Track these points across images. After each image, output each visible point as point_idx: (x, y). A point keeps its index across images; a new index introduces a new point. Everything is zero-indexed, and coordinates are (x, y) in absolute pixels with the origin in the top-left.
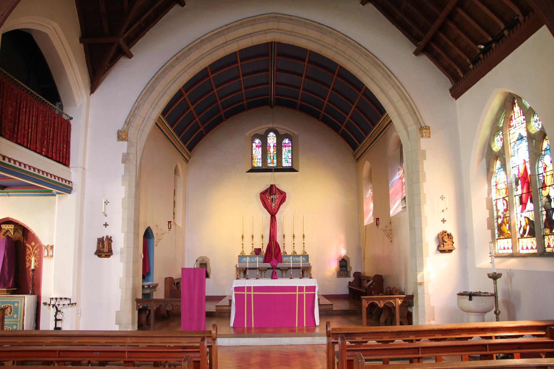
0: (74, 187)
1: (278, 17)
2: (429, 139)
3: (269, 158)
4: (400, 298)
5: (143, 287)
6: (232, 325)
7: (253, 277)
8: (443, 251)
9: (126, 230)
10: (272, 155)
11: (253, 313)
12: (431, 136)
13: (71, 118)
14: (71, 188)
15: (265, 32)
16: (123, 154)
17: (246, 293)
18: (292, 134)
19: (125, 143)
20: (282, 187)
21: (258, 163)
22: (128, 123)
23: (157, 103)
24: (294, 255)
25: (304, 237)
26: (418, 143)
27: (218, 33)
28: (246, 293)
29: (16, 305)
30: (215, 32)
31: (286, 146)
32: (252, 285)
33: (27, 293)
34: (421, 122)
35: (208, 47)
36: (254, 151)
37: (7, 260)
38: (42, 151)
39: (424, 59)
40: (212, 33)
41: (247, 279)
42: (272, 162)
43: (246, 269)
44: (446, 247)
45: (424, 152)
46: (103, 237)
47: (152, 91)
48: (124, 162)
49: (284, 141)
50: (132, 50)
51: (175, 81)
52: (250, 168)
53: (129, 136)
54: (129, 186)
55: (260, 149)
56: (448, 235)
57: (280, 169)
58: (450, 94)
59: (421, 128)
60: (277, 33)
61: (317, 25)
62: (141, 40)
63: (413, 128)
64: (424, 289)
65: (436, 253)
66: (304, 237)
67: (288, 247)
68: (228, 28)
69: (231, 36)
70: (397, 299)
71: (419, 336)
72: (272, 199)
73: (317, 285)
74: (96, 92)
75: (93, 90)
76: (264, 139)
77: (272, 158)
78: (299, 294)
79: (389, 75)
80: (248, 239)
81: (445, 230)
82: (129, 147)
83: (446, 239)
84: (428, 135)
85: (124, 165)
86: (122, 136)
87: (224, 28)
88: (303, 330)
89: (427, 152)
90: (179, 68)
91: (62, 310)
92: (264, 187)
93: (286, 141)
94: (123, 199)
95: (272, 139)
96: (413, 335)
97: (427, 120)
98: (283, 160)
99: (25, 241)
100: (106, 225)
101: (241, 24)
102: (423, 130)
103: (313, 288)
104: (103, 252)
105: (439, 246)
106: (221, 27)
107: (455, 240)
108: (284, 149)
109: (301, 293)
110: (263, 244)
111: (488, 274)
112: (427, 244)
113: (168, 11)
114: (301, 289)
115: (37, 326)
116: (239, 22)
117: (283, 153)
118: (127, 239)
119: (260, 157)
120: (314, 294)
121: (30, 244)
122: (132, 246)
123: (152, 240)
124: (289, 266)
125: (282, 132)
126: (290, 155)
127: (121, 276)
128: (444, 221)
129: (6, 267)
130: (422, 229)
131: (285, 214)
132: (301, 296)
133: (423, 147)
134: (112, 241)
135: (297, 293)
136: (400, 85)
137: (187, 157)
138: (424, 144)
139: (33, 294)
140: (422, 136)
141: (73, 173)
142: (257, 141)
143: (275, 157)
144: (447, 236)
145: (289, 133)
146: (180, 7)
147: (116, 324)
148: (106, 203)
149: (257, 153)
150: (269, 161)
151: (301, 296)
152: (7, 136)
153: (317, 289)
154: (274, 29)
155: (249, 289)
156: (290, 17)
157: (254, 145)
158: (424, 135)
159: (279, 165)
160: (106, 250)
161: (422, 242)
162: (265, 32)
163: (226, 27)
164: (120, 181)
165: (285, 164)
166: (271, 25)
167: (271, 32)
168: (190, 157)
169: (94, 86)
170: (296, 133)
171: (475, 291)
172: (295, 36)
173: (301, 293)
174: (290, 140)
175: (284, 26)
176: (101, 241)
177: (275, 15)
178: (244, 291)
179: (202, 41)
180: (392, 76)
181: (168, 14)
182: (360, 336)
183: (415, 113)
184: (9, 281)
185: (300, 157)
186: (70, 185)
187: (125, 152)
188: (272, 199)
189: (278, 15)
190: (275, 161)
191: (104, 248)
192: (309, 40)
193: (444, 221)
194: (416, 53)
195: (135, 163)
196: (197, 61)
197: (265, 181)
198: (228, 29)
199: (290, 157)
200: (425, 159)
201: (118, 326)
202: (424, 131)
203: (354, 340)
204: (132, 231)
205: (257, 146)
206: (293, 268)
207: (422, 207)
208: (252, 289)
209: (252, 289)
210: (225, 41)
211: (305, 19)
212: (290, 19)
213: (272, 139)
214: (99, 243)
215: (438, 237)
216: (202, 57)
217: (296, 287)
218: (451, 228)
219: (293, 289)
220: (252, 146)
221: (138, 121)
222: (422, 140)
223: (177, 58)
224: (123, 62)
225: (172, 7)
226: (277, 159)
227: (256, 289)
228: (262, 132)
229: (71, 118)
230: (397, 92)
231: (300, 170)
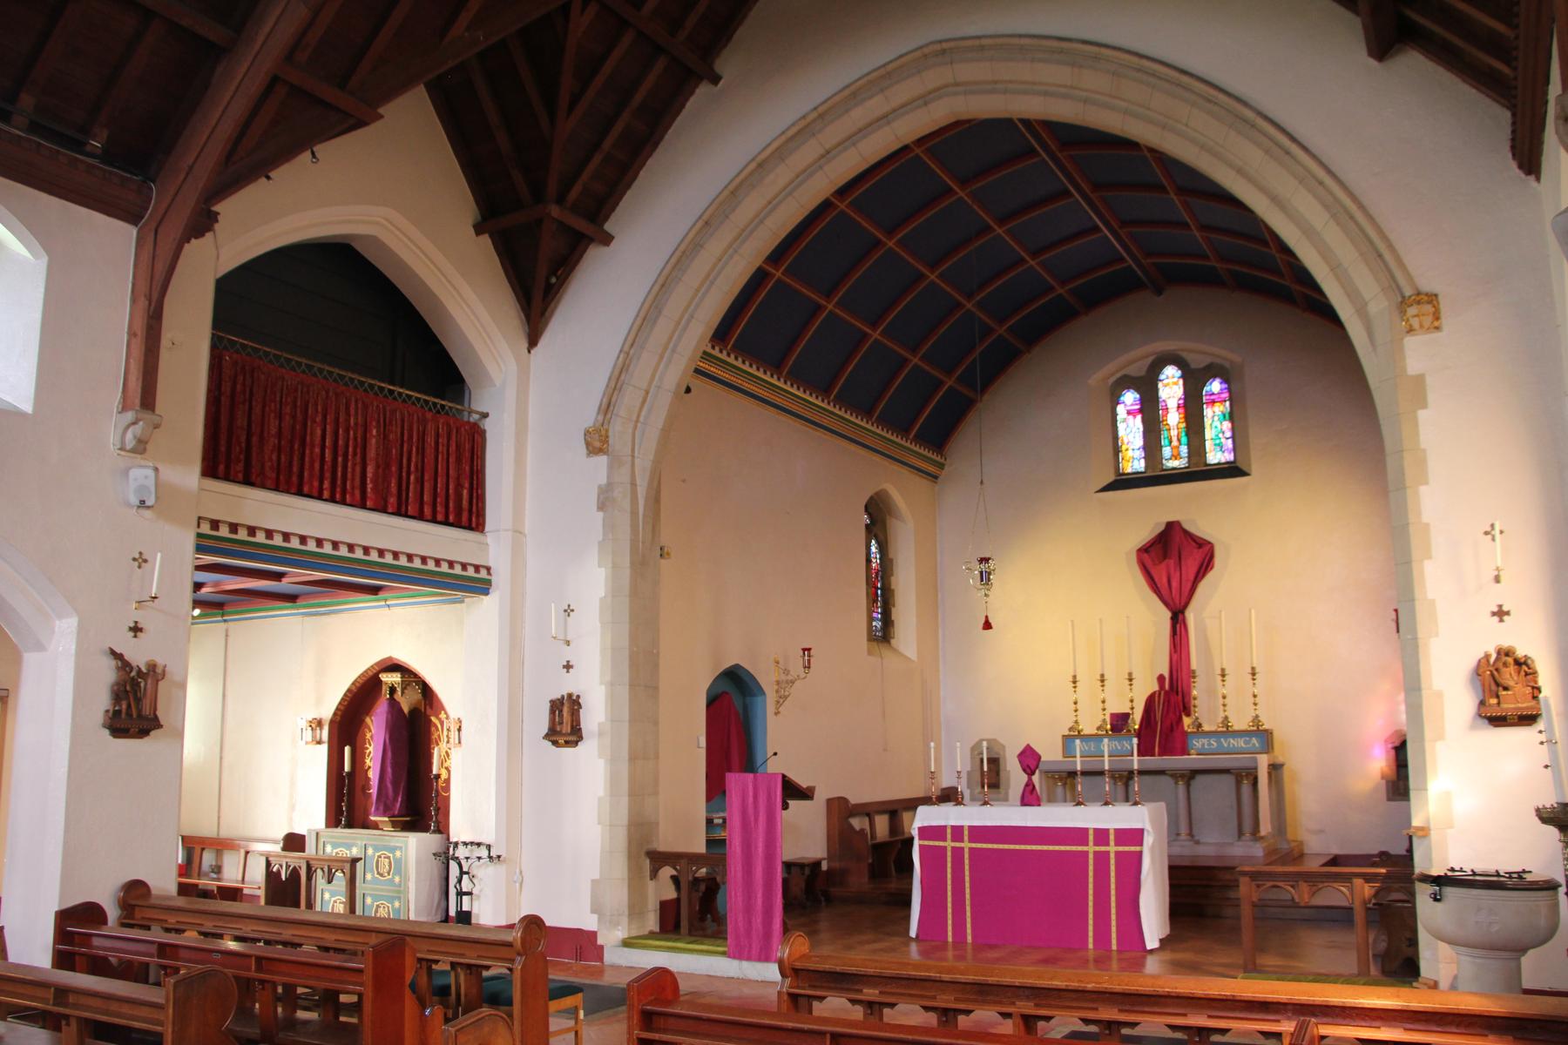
0: (494, 579)
1: (945, 52)
2: (1436, 335)
3: (1164, 442)
4: (1368, 878)
5: (709, 822)
6: (913, 934)
7: (1094, 800)
8: (1498, 721)
9: (608, 678)
10: (1174, 433)
11: (968, 902)
12: (1445, 321)
13: (485, 415)
14: (489, 582)
15: (925, 99)
16: (600, 487)
17: (949, 844)
18: (1227, 365)
19: (602, 460)
20: (1201, 526)
21: (1134, 461)
22: (607, 408)
23: (676, 346)
24: (1227, 731)
25: (1223, 675)
26: (1397, 354)
27: (799, 132)
28: (1091, 849)
29: (398, 854)
30: (790, 133)
31: (1213, 402)
32: (966, 823)
33: (425, 829)
34: (1402, 282)
35: (780, 176)
36: (1121, 427)
37: (389, 754)
38: (386, 502)
39: (1412, 64)
40: (784, 138)
41: (1079, 804)
42: (1174, 457)
43: (1131, 772)
44: (1509, 706)
45: (1420, 380)
46: (1487, 656)
47: (657, 317)
48: (601, 507)
49: (1206, 389)
50: (608, 227)
51: (712, 283)
52: (1111, 478)
53: (611, 441)
54: (615, 566)
55: (1139, 417)
56: (1518, 663)
57: (1199, 472)
58: (1514, 165)
59: (1403, 304)
60: (956, 94)
61: (1055, 44)
62: (629, 193)
63: (1379, 305)
64: (1429, 848)
65: (1473, 727)
66: (1223, 675)
67: (1221, 703)
68: (823, 115)
69: (833, 133)
70: (1358, 882)
71: (1049, 1006)
72: (1174, 563)
73: (1148, 826)
74: (544, 341)
75: (533, 342)
76: (1148, 390)
77: (1175, 443)
78: (1095, 853)
79: (1283, 140)
80: (1087, 681)
81: (1506, 643)
82: (611, 467)
83: (1509, 675)
84: (1427, 320)
85: (601, 514)
86: (597, 442)
87: (809, 119)
88: (1109, 958)
89: (1429, 380)
90: (714, 247)
91: (474, 871)
92: (1145, 532)
93: (1215, 386)
94: (601, 599)
95: (1171, 386)
96: (1028, 998)
97: (1426, 272)
98: (1208, 444)
99: (429, 711)
100: (568, 667)
101: (853, 95)
102: (1419, 306)
103: (1135, 836)
104: (560, 733)
105: (1482, 703)
106: (804, 117)
107: (1542, 681)
108: (1208, 412)
109: (1103, 849)
110: (1133, 699)
111: (1538, 810)
112: (1439, 695)
113: (683, 106)
114: (1102, 836)
115: (352, 910)
116: (847, 92)
117: (1207, 422)
118: (612, 698)
119: (1139, 442)
120: (1140, 853)
121: (437, 717)
122: (626, 717)
123: (759, 699)
124: (1070, 768)
125: (1197, 362)
126: (1227, 425)
127: (601, 793)
128: (1501, 614)
129: (389, 770)
130: (1417, 646)
131: (1212, 605)
132: (1102, 858)
133: (1413, 365)
134: (580, 706)
135: (1091, 849)
136: (1321, 174)
137: (931, 469)
138: (1418, 354)
139: (438, 831)
140: (1410, 330)
141: (490, 550)
142: (1130, 398)
143: (1184, 440)
144: (1512, 668)
145: (1218, 361)
146: (711, 87)
147: (593, 911)
148: (568, 611)
149: (1131, 431)
150: (1167, 452)
151: (1102, 858)
152: (269, 483)
153: (1148, 840)
154: (946, 86)
155: (957, 832)
156: (977, 42)
157: (1121, 410)
158: (1415, 323)
159: (1194, 460)
160: (567, 728)
161: (1419, 689)
162: (925, 99)
163: (815, 115)
164: (593, 556)
165: (1215, 457)
166: (934, 77)
167: (940, 98)
168: (941, 466)
169: (534, 326)
170: (1236, 358)
171: (1491, 868)
172: (1005, 92)
173: (1103, 849)
174: (1225, 380)
175: (970, 71)
176: (556, 706)
177: (938, 47)
178: (945, 840)
179: (760, 165)
180: (1294, 148)
181: (685, 112)
182: (874, 986)
183: (1380, 256)
184: (395, 800)
185: (1251, 431)
186: (483, 574)
187: (604, 481)
188: (1174, 563)
189: (945, 45)
190: (1184, 450)
191: (565, 723)
192: (1046, 94)
193: (1501, 614)
194: (1381, 48)
195: (627, 505)
196: (759, 219)
197: (1147, 513)
198: (821, 116)
199: (1228, 434)
200: (1424, 406)
201: (595, 917)
202: (1412, 311)
203: (935, 1004)
204: (626, 679)
205: (1129, 413)
206: (1084, 773)
207: (1415, 573)
208: (966, 832)
209: (966, 832)
210: (822, 151)
211: (1020, 36)
212: (980, 47)
213: (1171, 386)
214: (552, 712)
215: (1478, 671)
216: (772, 205)
217: (1086, 830)
218: (1530, 637)
219: (1078, 835)
220: (1114, 415)
221: (628, 401)
222: (1410, 342)
223: (708, 224)
224: (595, 254)
225: (692, 93)
226: (1189, 445)
227: (978, 833)
228: (1138, 369)
229: (485, 415)
230: (1316, 197)
231: (1255, 468)
